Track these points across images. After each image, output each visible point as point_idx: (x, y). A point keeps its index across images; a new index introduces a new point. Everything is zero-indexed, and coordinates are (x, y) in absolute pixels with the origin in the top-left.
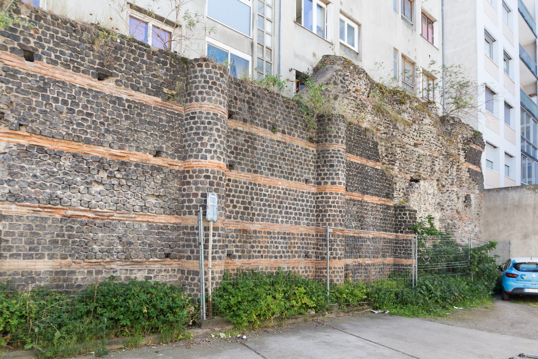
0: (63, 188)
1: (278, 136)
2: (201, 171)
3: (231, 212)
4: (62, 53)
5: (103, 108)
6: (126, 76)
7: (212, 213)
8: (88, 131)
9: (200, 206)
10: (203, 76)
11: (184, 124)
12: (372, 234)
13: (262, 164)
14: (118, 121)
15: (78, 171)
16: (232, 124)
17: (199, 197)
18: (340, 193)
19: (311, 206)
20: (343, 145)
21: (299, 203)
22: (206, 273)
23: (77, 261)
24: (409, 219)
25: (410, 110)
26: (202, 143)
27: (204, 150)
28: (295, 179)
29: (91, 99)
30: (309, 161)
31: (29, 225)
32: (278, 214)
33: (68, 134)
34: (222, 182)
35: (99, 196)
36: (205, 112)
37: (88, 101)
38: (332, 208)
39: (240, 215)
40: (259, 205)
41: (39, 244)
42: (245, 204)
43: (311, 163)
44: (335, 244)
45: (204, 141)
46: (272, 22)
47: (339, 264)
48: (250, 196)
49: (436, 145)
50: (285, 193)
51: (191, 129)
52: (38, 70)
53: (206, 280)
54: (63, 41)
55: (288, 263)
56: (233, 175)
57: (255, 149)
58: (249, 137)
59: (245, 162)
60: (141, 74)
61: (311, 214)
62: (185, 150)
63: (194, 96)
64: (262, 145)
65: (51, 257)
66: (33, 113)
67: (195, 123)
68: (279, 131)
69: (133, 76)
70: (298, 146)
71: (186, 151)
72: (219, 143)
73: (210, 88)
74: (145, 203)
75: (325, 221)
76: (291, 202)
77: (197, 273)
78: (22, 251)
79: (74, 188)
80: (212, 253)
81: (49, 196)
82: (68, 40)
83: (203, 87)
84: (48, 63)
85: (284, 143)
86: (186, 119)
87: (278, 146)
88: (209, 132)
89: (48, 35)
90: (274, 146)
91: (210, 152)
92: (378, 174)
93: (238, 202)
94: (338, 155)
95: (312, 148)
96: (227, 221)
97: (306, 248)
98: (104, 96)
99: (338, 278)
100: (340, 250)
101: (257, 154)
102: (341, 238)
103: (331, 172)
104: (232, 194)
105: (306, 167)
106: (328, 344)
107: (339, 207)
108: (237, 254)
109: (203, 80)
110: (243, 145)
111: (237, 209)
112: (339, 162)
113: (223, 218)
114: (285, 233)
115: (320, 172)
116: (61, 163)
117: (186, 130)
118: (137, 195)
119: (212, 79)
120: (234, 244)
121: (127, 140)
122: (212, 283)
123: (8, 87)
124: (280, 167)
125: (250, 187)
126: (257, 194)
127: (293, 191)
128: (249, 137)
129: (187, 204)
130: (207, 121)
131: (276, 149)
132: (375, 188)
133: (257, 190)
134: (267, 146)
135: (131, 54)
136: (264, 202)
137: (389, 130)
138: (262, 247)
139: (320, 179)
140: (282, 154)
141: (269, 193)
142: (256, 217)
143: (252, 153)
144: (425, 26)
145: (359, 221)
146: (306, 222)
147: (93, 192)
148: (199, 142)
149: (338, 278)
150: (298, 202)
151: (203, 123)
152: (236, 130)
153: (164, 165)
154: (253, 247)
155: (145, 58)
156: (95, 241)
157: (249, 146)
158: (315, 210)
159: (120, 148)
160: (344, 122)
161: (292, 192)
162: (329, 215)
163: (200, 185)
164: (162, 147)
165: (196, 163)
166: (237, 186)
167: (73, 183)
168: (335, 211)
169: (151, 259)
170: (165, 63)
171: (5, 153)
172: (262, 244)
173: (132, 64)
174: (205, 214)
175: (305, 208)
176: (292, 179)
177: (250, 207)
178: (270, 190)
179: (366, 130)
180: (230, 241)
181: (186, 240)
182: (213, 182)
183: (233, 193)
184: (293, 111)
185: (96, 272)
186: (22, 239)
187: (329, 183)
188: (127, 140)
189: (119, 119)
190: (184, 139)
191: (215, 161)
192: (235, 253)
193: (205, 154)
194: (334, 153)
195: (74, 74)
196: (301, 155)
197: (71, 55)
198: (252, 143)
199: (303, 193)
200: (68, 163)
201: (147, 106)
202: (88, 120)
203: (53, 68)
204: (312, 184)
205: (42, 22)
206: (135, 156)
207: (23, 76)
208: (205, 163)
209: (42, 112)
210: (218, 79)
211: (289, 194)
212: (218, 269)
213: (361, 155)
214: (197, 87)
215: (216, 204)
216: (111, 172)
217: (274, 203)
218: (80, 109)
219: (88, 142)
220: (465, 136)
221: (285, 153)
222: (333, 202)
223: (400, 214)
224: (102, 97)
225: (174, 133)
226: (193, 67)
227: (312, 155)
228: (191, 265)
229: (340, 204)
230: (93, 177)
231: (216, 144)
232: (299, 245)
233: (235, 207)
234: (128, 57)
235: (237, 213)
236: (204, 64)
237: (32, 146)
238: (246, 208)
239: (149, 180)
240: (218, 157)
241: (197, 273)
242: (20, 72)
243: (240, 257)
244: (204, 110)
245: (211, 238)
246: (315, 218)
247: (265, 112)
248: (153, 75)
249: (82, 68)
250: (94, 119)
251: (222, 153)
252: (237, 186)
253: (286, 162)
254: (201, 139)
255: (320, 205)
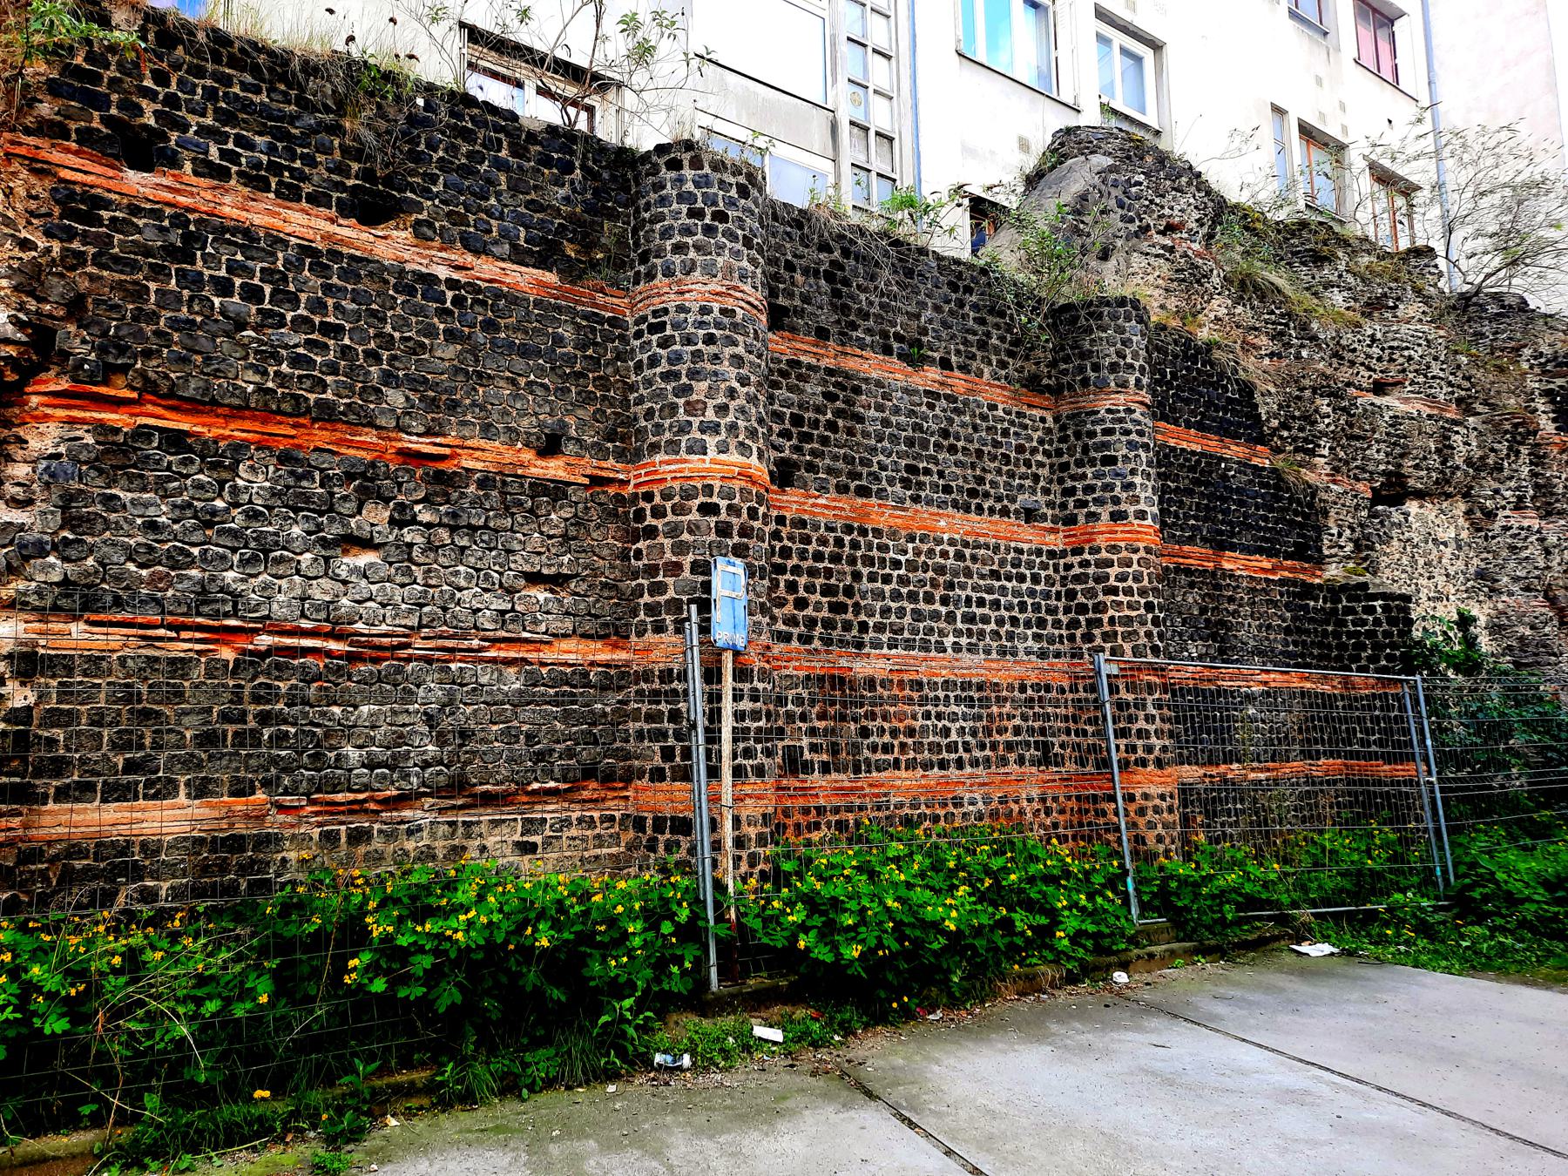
0: (244, 563)
1: (931, 376)
2: (688, 495)
3: (791, 621)
4: (241, 141)
5: (374, 306)
6: (446, 209)
7: (729, 626)
8: (329, 379)
9: (690, 602)
10: (681, 198)
11: (633, 350)
12: (1255, 678)
13: (883, 467)
14: (422, 345)
15: (298, 504)
16: (781, 345)
17: (686, 573)
18: (1141, 545)
19: (1047, 596)
20: (1143, 392)
21: (1009, 585)
22: (714, 825)
23: (288, 800)
24: (1385, 627)
25: (1350, 279)
26: (688, 403)
27: (695, 425)
28: (992, 511)
29: (335, 280)
30: (1034, 451)
31: (127, 685)
32: (943, 625)
33: (260, 389)
34: (756, 524)
35: (364, 583)
36: (695, 307)
37: (327, 289)
38: (1122, 597)
39: (819, 629)
40: (880, 595)
41: (157, 746)
42: (835, 594)
43: (1040, 457)
44: (1141, 714)
45: (694, 397)
46: (889, 58)
47: (1154, 784)
48: (847, 569)
49: (1450, 384)
50: (960, 556)
51: (654, 361)
52: (169, 196)
53: (717, 846)
54: (247, 106)
55: (984, 784)
56: (792, 501)
57: (860, 419)
58: (836, 384)
59: (827, 461)
60: (493, 201)
61: (1049, 618)
62: (638, 431)
63: (658, 261)
64: (880, 408)
65: (201, 790)
66: (149, 329)
67: (664, 343)
68: (932, 361)
69: (467, 210)
70: (993, 407)
71: (641, 433)
72: (741, 401)
73: (709, 230)
74: (512, 600)
75: (1098, 641)
76: (982, 582)
77: (683, 826)
78: (99, 774)
79: (279, 561)
80: (735, 757)
81: (198, 588)
82: (262, 103)
83: (687, 231)
84: (196, 173)
85: (948, 398)
86: (639, 335)
87: (931, 407)
88: (709, 366)
89: (199, 91)
90: (917, 409)
91: (714, 429)
92: (1262, 485)
93: (810, 588)
94: (1129, 426)
95: (1040, 414)
96: (778, 648)
97: (1043, 731)
98: (377, 270)
99: (1160, 830)
100: (1159, 734)
101: (866, 435)
102: (1157, 696)
103: (1108, 480)
104: (790, 563)
105: (1023, 469)
106: (1169, 1081)
107: (1143, 592)
108: (818, 758)
109: (684, 208)
110: (819, 410)
111: (809, 611)
112: (1132, 445)
113: (765, 639)
114: (966, 686)
115: (1069, 484)
116: (240, 483)
117: (639, 367)
118: (487, 577)
119: (715, 203)
120: (804, 726)
121: (453, 406)
122: (738, 859)
123: (68, 249)
124: (941, 474)
125: (847, 538)
126: (869, 561)
127: (987, 547)
128: (836, 384)
129: (647, 598)
130: (701, 332)
131: (925, 418)
132: (1260, 529)
133: (870, 547)
134: (896, 411)
135: (459, 141)
136: (894, 585)
137: (1288, 345)
138: (894, 733)
139: (1071, 505)
140: (945, 434)
141: (910, 556)
142: (871, 634)
143: (850, 432)
144: (1367, 34)
145: (1214, 636)
146: (1036, 646)
147: (343, 572)
148: (681, 401)
149: (1160, 830)
150: (1004, 582)
151: (689, 341)
152: (794, 364)
153: (572, 479)
154: (865, 733)
155: (504, 153)
156: (348, 730)
157: (839, 413)
158: (1061, 605)
159: (428, 432)
160: (1140, 321)
161: (982, 551)
162: (1112, 620)
163: (686, 536)
164: (565, 426)
165: (673, 467)
166: (807, 540)
167: (276, 543)
168: (1130, 606)
169: (536, 786)
170: (568, 168)
171: (58, 456)
172: (896, 724)
173: (465, 171)
174: (705, 629)
175: (1030, 601)
176: (980, 509)
177: (849, 602)
178: (910, 546)
179: (1210, 346)
180: (790, 717)
181: (650, 717)
182: (729, 525)
183: (795, 561)
184: (974, 298)
185: (349, 837)
186: (100, 735)
187: (1105, 517)
188: (453, 406)
189: (427, 341)
190: (632, 397)
191: (734, 457)
192: (807, 755)
193: (698, 435)
194: (1113, 421)
195: (280, 206)
196: (1005, 433)
197: (271, 149)
198: (847, 401)
199: (1020, 551)
200: (261, 482)
201: (514, 300)
202: (326, 346)
203: (214, 188)
204: (1048, 524)
205: (180, 51)
206: (478, 454)
207: (117, 214)
208: (701, 465)
209: (175, 323)
210: (732, 203)
211: (974, 558)
212: (750, 809)
213: (1200, 427)
214: (666, 234)
215: (742, 592)
216: (401, 507)
217: (928, 588)
218: (302, 311)
219: (326, 414)
220: (1545, 349)
221: (955, 428)
222: (1122, 578)
223: (1349, 611)
224: (371, 274)
225: (600, 378)
226: (655, 171)
227: (1040, 433)
228: (665, 798)
229: (1146, 582)
230: (346, 525)
231: (733, 405)
232: (1017, 721)
233: (801, 604)
234: (452, 149)
235: (811, 623)
236: (686, 157)
237: (143, 433)
238: (837, 608)
239: (525, 529)
240: (742, 444)
241: (683, 826)
242: (107, 205)
243: (826, 768)
244: (693, 301)
245: (728, 706)
246: (1064, 632)
247: (882, 306)
248: (530, 204)
249: (307, 188)
250: (347, 341)
251: (752, 434)
252: (807, 540)
253: (960, 456)
254: (686, 390)
255: (1078, 588)
